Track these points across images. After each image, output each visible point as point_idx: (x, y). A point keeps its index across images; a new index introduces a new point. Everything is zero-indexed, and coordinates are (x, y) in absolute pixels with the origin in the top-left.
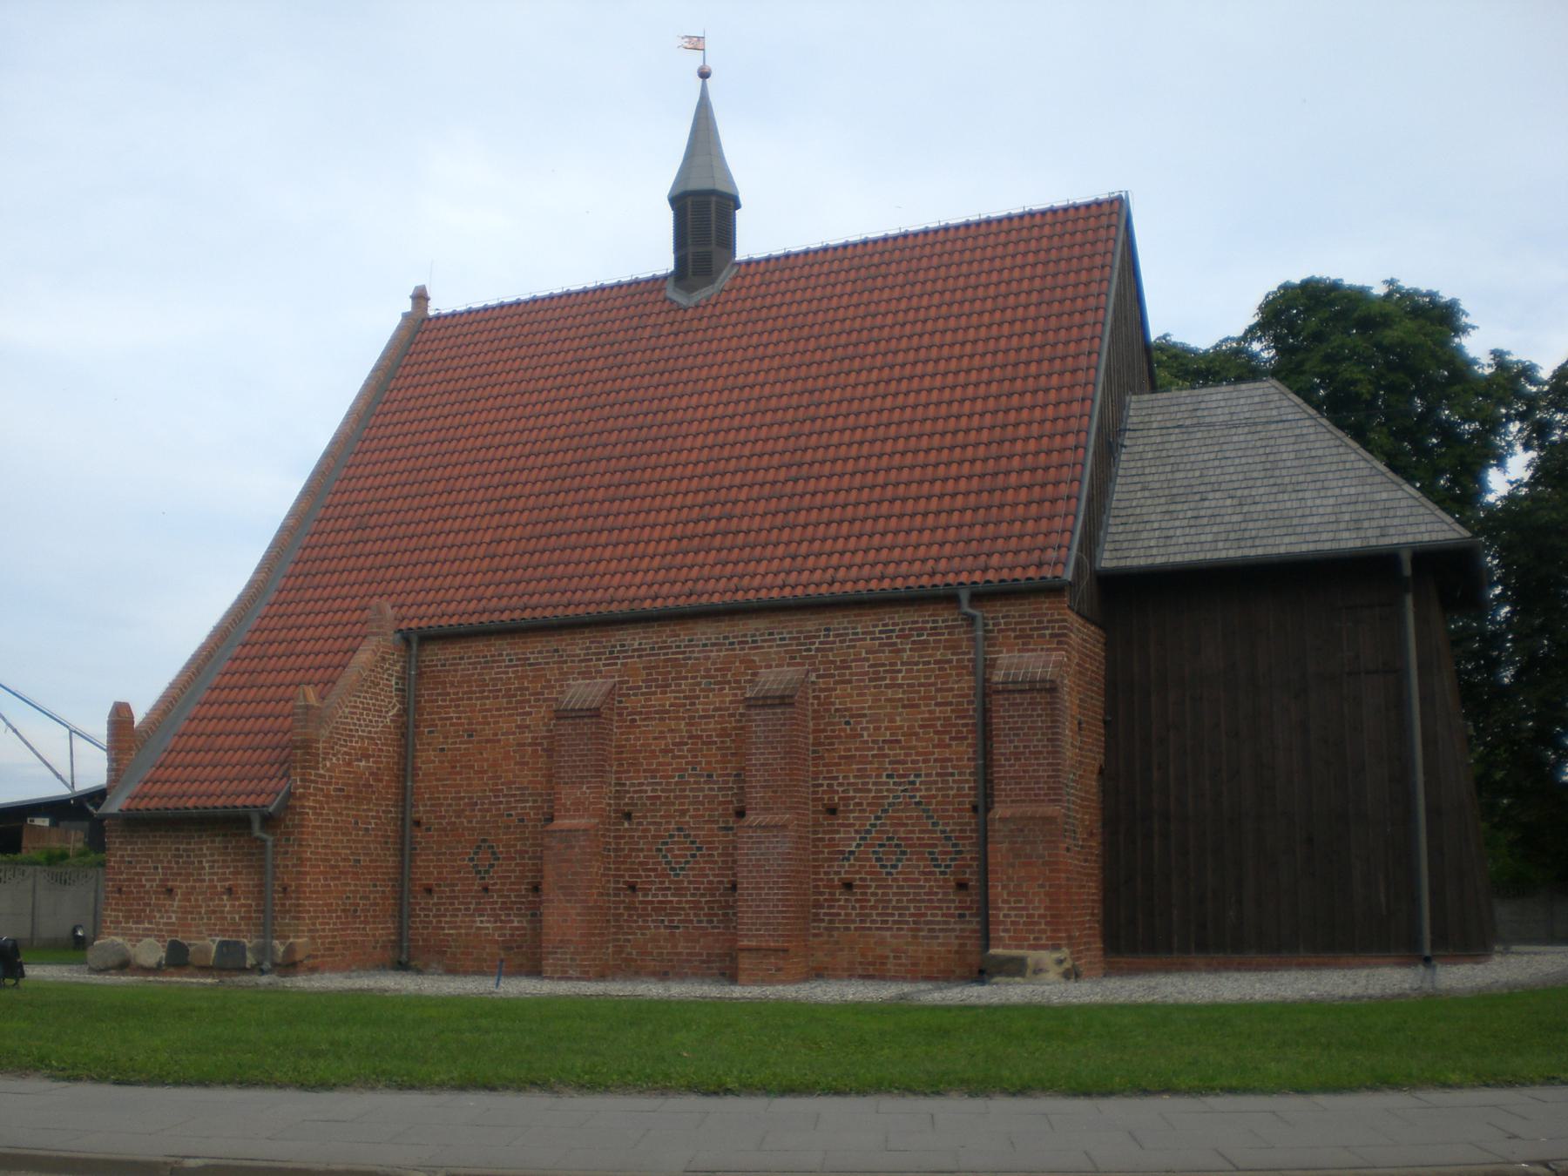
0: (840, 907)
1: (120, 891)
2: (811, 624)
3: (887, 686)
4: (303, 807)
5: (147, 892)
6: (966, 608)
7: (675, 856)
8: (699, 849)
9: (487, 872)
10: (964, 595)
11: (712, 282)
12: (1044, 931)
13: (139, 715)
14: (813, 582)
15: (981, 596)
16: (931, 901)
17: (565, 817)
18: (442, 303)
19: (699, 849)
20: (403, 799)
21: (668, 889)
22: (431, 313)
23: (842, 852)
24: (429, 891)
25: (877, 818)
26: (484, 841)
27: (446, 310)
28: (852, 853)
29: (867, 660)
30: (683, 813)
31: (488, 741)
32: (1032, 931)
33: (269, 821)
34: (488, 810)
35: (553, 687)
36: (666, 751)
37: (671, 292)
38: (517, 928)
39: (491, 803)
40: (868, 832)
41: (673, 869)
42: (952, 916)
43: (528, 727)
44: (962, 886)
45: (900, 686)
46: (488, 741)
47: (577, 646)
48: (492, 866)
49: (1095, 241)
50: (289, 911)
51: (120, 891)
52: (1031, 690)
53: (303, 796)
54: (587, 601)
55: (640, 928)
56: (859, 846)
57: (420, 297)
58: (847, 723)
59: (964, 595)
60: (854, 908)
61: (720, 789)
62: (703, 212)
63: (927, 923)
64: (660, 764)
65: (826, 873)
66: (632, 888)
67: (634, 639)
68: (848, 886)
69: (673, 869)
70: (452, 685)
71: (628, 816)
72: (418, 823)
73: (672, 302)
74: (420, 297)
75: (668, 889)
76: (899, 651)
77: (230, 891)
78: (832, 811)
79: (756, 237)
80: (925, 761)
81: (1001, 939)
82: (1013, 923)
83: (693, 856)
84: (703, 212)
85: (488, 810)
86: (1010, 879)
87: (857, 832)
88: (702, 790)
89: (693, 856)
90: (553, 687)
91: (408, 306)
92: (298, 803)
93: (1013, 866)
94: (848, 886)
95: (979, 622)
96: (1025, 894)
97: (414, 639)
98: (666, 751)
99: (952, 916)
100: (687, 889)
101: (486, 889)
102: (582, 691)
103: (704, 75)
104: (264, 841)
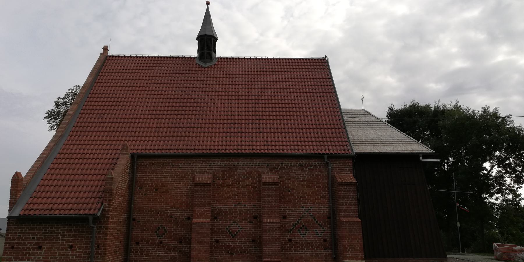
0: (288, 247)
1: (13, 247)
2: (277, 162)
3: (301, 181)
4: (109, 214)
5: (29, 248)
6: (326, 160)
7: (233, 231)
8: (241, 229)
9: (162, 236)
10: (326, 157)
11: (212, 61)
12: (359, 255)
13: (23, 175)
14: (275, 149)
15: (331, 157)
16: (316, 245)
17: (197, 218)
18: (113, 51)
19: (241, 229)
20: (129, 212)
21: (230, 241)
22: (109, 54)
23: (288, 230)
24: (138, 243)
25: (299, 220)
26: (161, 226)
27: (115, 54)
28: (291, 230)
29: (295, 173)
30: (236, 217)
31: (163, 192)
32: (356, 255)
33: (96, 219)
34: (163, 215)
35: (189, 175)
36: (229, 198)
37: (198, 62)
38: (173, 256)
39: (164, 213)
40: (297, 224)
41: (232, 235)
42: (323, 249)
43: (179, 188)
44: (325, 240)
45: (305, 181)
46: (163, 192)
47: (198, 163)
48: (164, 234)
49: (316, 72)
50: (100, 254)
51: (13, 247)
52: (349, 185)
53: (109, 210)
54: (200, 149)
55: (220, 254)
56: (293, 228)
57: (105, 49)
58: (289, 191)
59: (326, 157)
60: (292, 247)
61: (248, 210)
62: (207, 40)
63: (315, 251)
64: (227, 201)
65: (283, 236)
66: (217, 241)
67: (218, 162)
68: (290, 240)
69: (232, 235)
70: (149, 173)
71: (216, 218)
72: (134, 220)
73: (199, 65)
74: (105, 49)
75: (230, 241)
76: (304, 171)
77: (71, 247)
78: (285, 217)
79: (222, 50)
80: (313, 203)
81: (348, 257)
82: (351, 252)
83: (239, 231)
84: (207, 40)
85: (163, 215)
86: (349, 239)
87: (293, 224)
88: (242, 210)
89: (239, 231)
90: (189, 175)
91: (102, 51)
92: (106, 213)
93: (350, 235)
94: (290, 240)
95: (330, 164)
96: (354, 244)
97: (136, 157)
98: (229, 198)
99: (323, 249)
100: (237, 241)
101: (161, 243)
102: (269, 177)
103: (208, 3)
104: (93, 227)
